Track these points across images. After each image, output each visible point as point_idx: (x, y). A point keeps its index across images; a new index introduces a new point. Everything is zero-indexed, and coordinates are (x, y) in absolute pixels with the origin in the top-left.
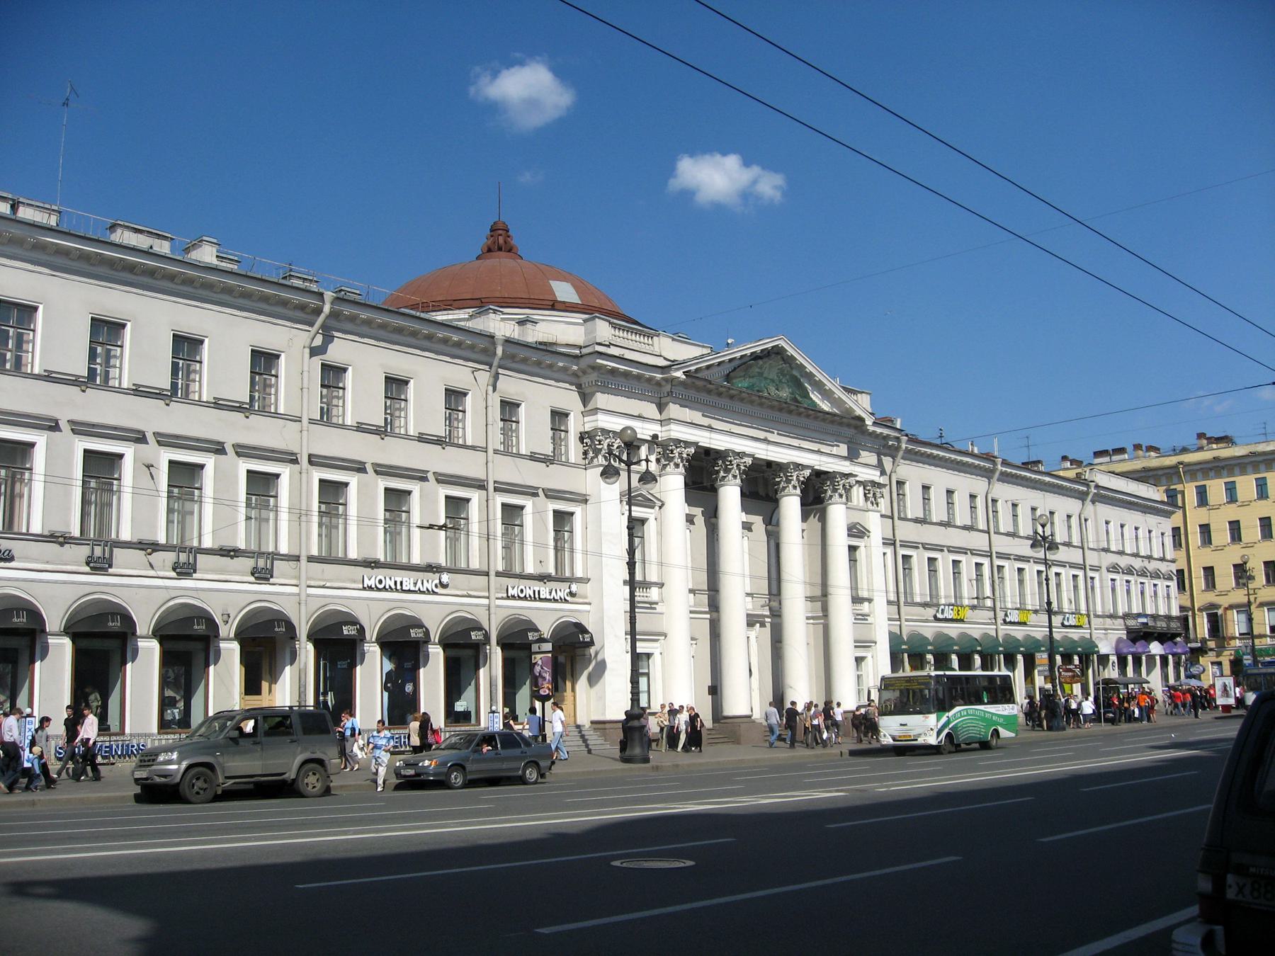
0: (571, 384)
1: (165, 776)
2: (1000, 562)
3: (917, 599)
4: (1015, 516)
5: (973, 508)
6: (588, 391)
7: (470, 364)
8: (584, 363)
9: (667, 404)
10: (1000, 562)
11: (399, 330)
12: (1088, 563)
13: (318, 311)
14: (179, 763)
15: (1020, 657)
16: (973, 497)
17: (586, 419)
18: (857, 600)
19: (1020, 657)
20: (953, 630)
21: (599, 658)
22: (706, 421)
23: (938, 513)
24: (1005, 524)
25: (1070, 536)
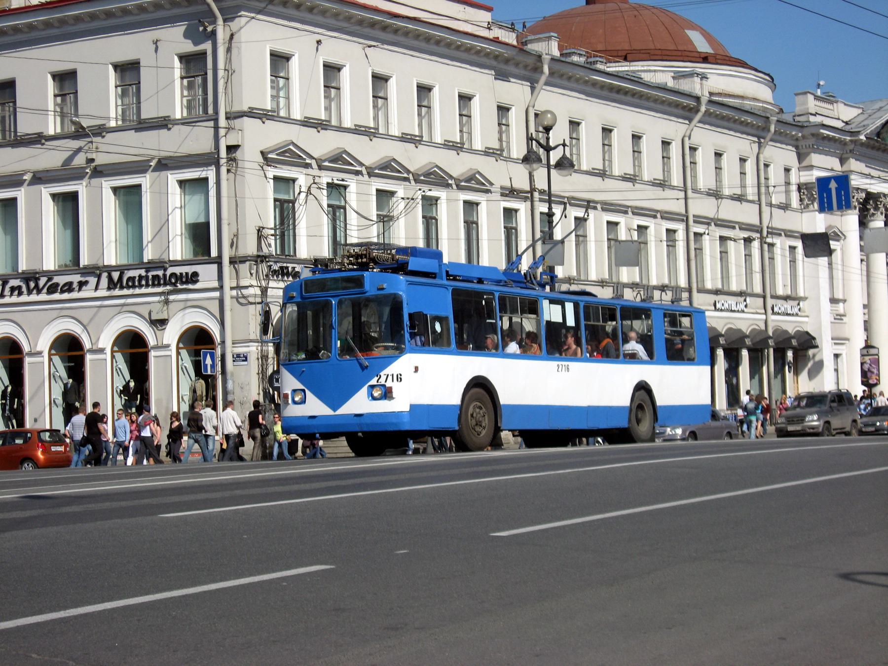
0: (793, 146)
1: (813, 429)
2: (700, 229)
3: (709, 285)
4: (718, 168)
5: (666, 158)
6: (802, 151)
7: (750, 138)
8: (807, 132)
9: (848, 159)
10: (700, 229)
11: (723, 118)
12: (692, 211)
13: (698, 111)
14: (818, 420)
15: (745, 353)
16: (666, 144)
17: (802, 173)
18: (834, 301)
19: (745, 353)
20: (777, 322)
21: (817, 358)
22: (867, 171)
23: (621, 164)
24: (705, 179)
25: (743, 186)
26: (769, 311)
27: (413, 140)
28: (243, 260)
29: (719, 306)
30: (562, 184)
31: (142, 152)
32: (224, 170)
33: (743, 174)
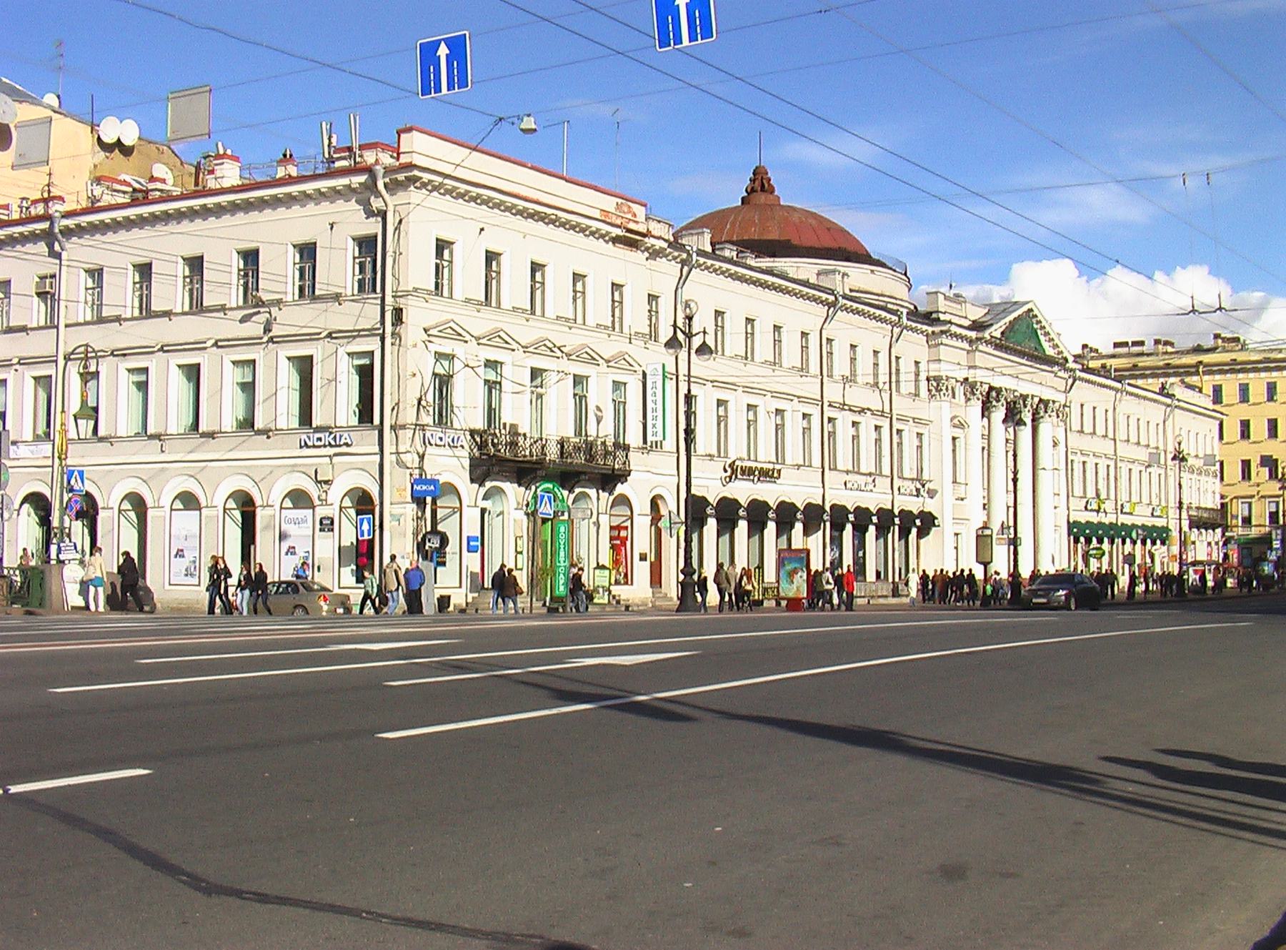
5: (804, 348)
26: (896, 492)
27: (570, 322)
28: (403, 427)
29: (849, 485)
30: (701, 366)
31: (144, 253)
32: (388, 341)
33: (876, 365)
